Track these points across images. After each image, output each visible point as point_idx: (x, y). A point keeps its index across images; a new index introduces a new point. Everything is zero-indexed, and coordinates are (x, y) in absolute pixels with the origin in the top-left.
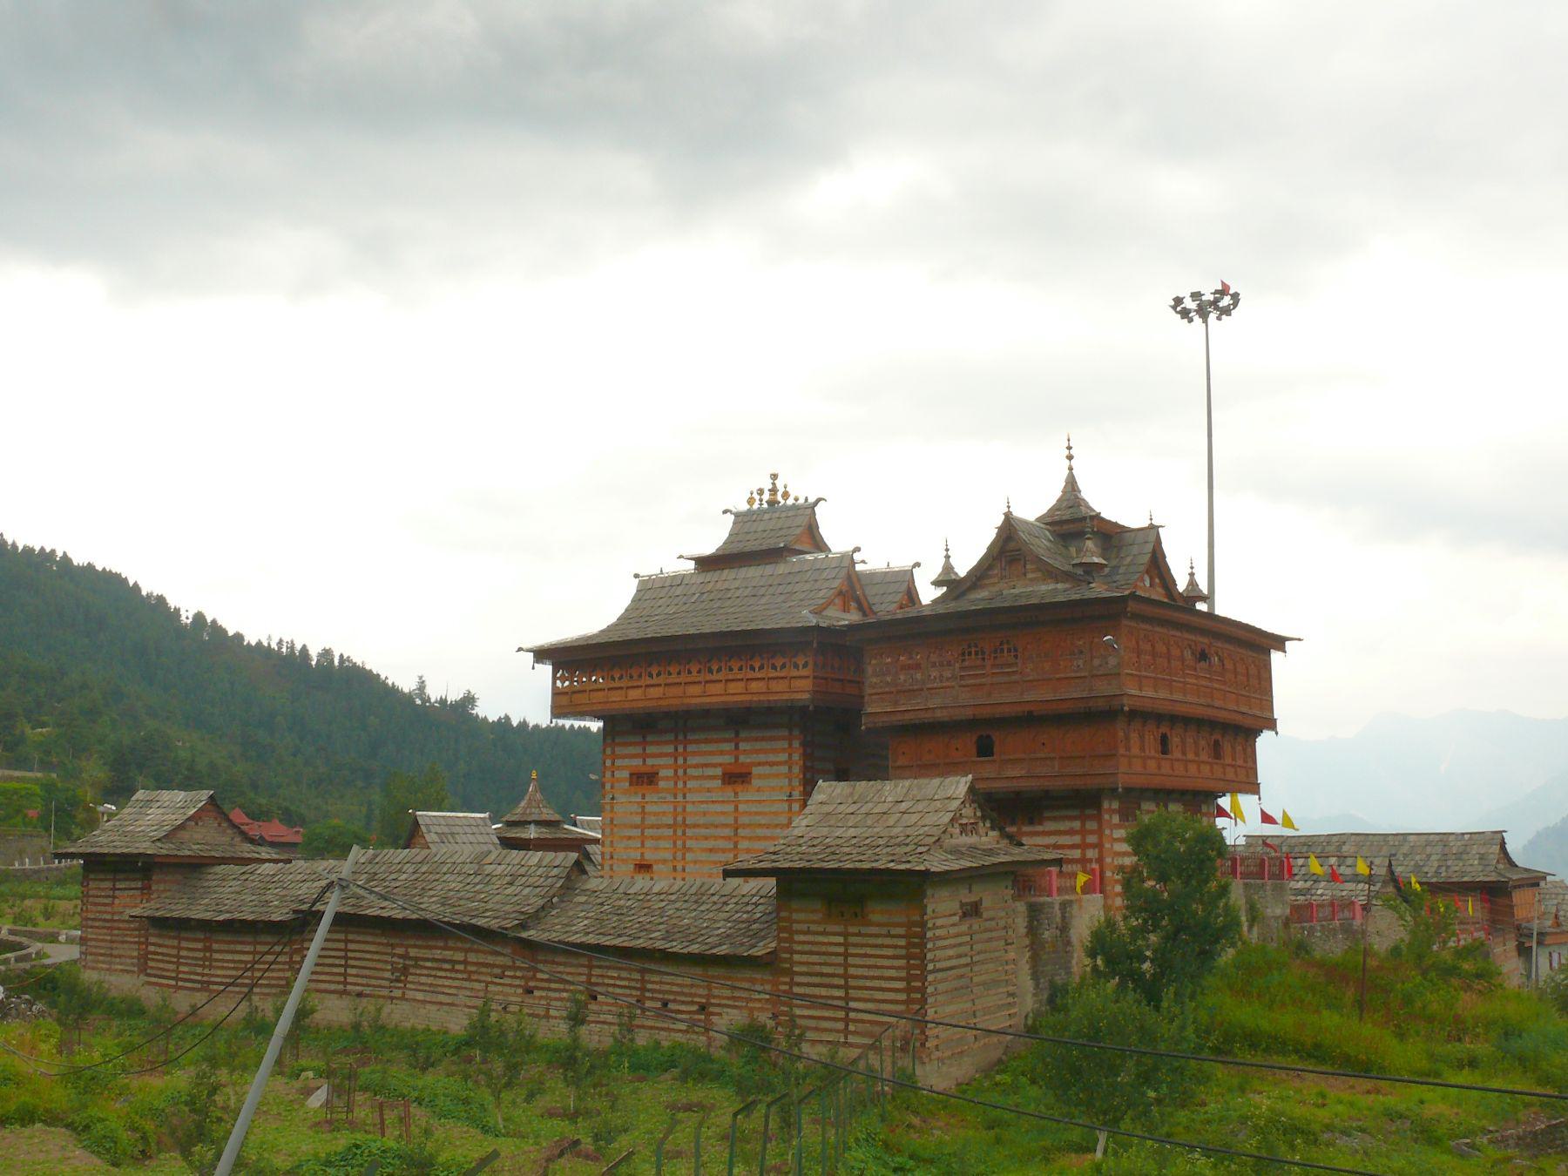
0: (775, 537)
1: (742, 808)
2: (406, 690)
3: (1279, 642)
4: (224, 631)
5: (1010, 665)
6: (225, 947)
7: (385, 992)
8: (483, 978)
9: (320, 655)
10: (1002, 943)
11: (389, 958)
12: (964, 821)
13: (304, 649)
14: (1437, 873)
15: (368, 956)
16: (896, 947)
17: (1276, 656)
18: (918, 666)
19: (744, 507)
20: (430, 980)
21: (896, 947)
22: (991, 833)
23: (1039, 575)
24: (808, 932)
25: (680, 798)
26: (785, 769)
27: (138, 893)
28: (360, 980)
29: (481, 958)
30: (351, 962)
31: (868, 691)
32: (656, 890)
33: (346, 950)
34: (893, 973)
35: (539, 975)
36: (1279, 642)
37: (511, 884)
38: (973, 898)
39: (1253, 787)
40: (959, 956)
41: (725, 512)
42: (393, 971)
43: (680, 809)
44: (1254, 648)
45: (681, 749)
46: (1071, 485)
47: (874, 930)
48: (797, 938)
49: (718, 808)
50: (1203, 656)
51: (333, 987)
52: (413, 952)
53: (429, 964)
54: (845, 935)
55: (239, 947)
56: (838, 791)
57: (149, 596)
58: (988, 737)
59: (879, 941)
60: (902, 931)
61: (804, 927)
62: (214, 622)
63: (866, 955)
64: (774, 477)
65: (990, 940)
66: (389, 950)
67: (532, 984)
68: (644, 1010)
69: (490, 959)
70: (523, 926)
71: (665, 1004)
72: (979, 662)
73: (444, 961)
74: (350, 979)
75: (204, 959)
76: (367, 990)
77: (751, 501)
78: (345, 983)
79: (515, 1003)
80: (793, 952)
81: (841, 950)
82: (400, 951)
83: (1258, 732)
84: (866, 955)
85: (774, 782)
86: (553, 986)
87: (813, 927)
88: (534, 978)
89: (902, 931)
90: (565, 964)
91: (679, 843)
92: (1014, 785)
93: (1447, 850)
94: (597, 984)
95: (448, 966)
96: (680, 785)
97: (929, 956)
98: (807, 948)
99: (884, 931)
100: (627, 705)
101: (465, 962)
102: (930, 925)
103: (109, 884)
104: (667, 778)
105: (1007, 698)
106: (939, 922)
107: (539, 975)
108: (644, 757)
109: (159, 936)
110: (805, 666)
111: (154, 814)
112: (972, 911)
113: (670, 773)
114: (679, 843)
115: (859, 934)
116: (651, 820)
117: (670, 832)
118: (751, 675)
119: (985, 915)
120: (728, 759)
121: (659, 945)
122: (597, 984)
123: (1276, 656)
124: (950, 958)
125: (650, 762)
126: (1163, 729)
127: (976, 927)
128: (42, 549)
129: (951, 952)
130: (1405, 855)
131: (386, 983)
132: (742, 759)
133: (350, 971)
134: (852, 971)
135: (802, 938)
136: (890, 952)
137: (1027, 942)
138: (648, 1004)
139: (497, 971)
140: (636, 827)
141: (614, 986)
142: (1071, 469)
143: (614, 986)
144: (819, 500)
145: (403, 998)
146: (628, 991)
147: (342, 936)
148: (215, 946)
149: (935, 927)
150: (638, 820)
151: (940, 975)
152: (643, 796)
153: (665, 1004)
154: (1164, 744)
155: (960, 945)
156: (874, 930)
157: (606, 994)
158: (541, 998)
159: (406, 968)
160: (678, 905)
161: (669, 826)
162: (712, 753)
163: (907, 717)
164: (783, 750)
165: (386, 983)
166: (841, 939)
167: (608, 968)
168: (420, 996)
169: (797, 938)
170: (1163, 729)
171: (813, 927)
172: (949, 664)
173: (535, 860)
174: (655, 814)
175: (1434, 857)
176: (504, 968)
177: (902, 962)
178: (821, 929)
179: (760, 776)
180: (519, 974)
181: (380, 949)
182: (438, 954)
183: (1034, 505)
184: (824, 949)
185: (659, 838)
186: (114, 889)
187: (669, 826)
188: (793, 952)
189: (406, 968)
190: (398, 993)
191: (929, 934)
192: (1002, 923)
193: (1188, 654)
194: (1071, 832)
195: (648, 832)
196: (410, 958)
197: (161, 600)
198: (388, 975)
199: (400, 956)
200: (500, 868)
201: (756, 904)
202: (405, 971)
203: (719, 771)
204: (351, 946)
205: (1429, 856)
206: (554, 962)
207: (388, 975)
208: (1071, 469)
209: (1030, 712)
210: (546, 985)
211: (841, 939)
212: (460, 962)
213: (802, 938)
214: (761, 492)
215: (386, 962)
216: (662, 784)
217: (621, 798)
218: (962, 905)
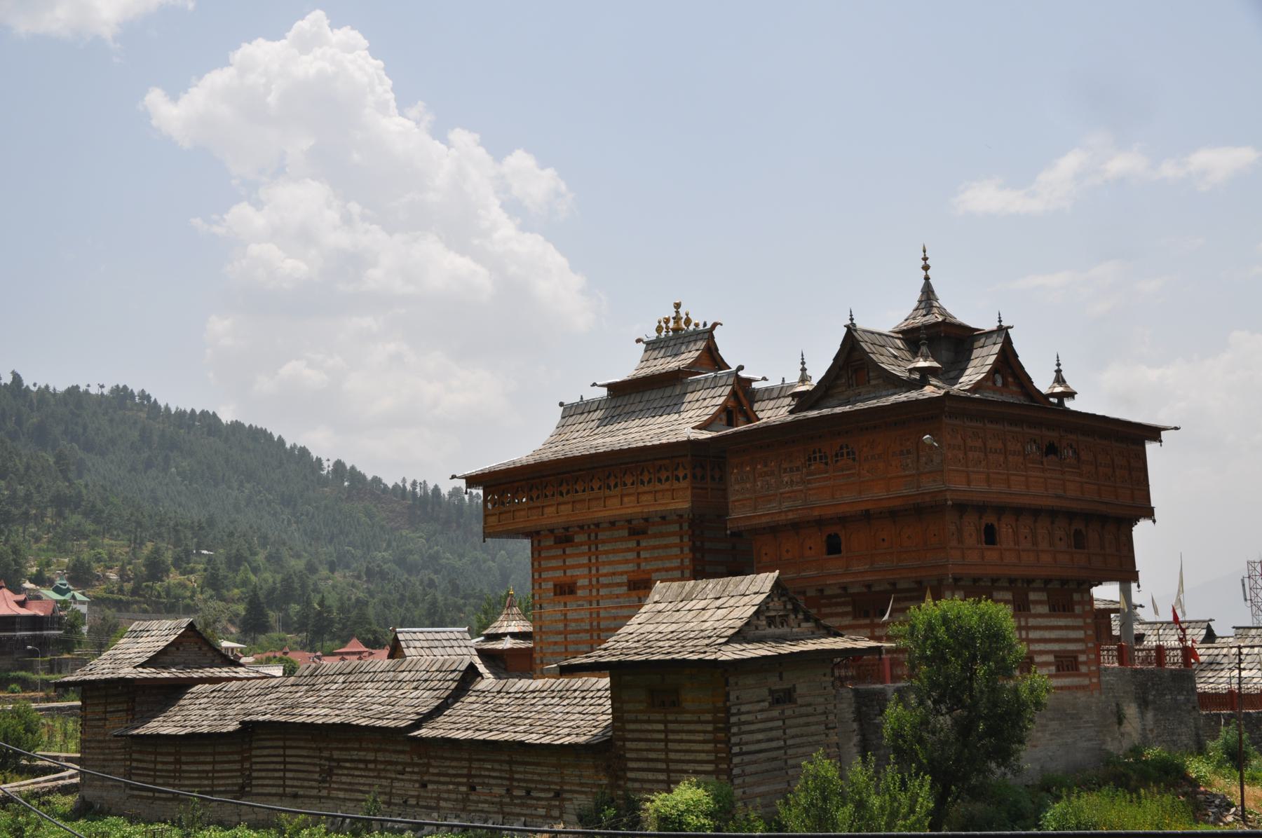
0: (686, 356)
3: (1154, 433)
4: (364, 477)
6: (190, 759)
7: (314, 792)
8: (389, 775)
9: (451, 495)
10: (823, 727)
11: (316, 761)
12: (772, 614)
15: (301, 760)
16: (705, 732)
17: (1151, 448)
19: (653, 335)
20: (348, 780)
21: (705, 732)
22: (804, 625)
23: (881, 381)
24: (636, 721)
25: (594, 605)
27: (123, 714)
28: (296, 783)
29: (388, 757)
30: (289, 766)
31: (732, 499)
32: (531, 688)
33: (285, 756)
34: (703, 756)
35: (432, 770)
36: (1154, 433)
37: (416, 688)
40: (771, 740)
41: (638, 341)
42: (320, 773)
43: (594, 615)
46: (928, 294)
47: (687, 717)
51: (274, 790)
52: (336, 754)
53: (348, 765)
55: (202, 758)
57: (294, 447)
58: (837, 535)
59: (692, 727)
60: (708, 717)
61: (632, 716)
62: (353, 468)
64: (677, 306)
65: (807, 725)
66: (317, 754)
67: (426, 778)
68: (513, 797)
69: (394, 758)
70: (417, 725)
71: (528, 793)
73: (360, 761)
74: (288, 782)
75: (174, 771)
76: (301, 792)
77: (659, 329)
78: (284, 786)
79: (412, 796)
80: (625, 740)
81: (662, 736)
82: (326, 754)
86: (442, 779)
87: (641, 717)
88: (427, 772)
89: (708, 717)
90: (452, 759)
94: (475, 776)
95: (362, 766)
96: (594, 592)
97: (734, 740)
98: (636, 735)
101: (375, 761)
102: (734, 710)
103: (100, 709)
104: (583, 587)
106: (744, 708)
107: (432, 770)
108: (565, 568)
109: (140, 752)
110: (685, 477)
112: (783, 698)
113: (586, 582)
115: (676, 722)
119: (799, 701)
122: (475, 776)
123: (1151, 448)
125: (569, 573)
126: (990, 519)
127: (788, 712)
128: (193, 411)
129: (760, 736)
131: (314, 784)
132: (643, 565)
133: (289, 775)
134: (672, 756)
135: (632, 726)
136: (701, 737)
138: (516, 793)
139: (400, 768)
140: (560, 633)
141: (490, 777)
142: (927, 278)
143: (490, 777)
144: (715, 325)
145: (328, 798)
146: (499, 782)
147: (281, 743)
148: (184, 759)
149: (739, 713)
150: (561, 626)
151: (747, 758)
152: (565, 605)
153: (528, 793)
154: (990, 536)
155: (771, 729)
156: (687, 717)
157: (483, 784)
158: (433, 791)
159: (331, 769)
160: (545, 701)
161: (586, 631)
162: (619, 562)
163: (764, 520)
165: (314, 784)
166: (661, 727)
167: (484, 760)
168: (341, 795)
171: (641, 717)
174: (576, 620)
176: (405, 764)
177: (710, 747)
178: (645, 718)
180: (416, 770)
181: (311, 753)
182: (355, 755)
183: (888, 313)
186: (106, 712)
187: (586, 631)
188: (625, 740)
189: (331, 769)
190: (324, 793)
191: (733, 719)
192: (820, 709)
195: (571, 637)
196: (334, 760)
197: (304, 452)
198: (316, 776)
199: (326, 759)
202: (330, 772)
203: (624, 579)
204: (289, 752)
206: (443, 758)
207: (316, 776)
208: (927, 278)
210: (436, 779)
211: (661, 727)
212: (371, 762)
213: (632, 726)
214: (667, 321)
215: (314, 765)
216: (580, 593)
218: (771, 692)
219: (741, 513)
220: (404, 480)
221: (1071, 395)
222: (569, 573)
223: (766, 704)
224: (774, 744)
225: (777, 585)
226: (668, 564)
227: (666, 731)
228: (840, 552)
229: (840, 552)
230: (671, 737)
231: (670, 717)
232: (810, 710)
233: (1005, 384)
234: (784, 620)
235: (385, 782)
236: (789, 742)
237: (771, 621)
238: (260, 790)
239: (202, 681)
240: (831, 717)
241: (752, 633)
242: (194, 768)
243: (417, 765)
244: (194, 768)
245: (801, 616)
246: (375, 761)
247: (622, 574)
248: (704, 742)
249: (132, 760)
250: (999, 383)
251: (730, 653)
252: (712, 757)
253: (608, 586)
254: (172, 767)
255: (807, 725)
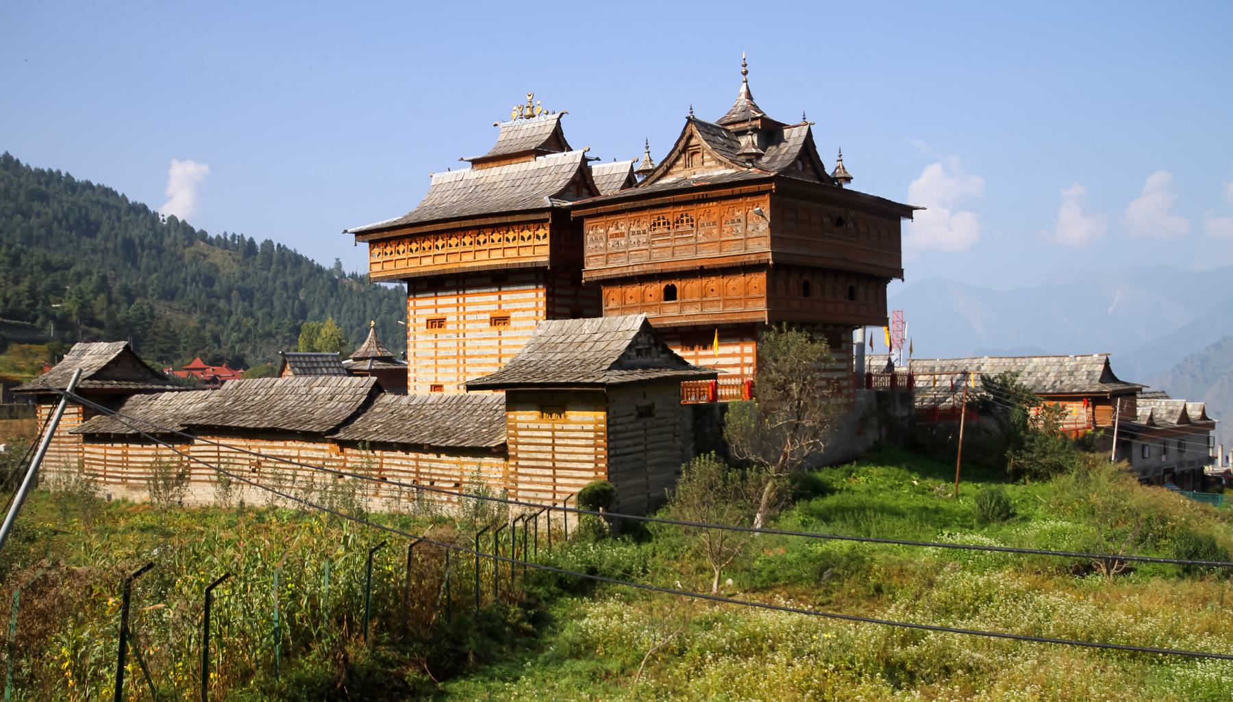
1: (503, 342)
2: (327, 268)
3: (907, 211)
4: (192, 230)
5: (688, 232)
9: (262, 245)
13: (251, 240)
14: (1053, 387)
16: (587, 439)
17: (905, 223)
18: (622, 235)
21: (587, 439)
24: (528, 429)
26: (533, 313)
36: (907, 211)
38: (647, 402)
39: (882, 321)
40: (636, 445)
44: (891, 215)
45: (461, 300)
48: (521, 433)
49: (488, 343)
50: (840, 222)
52: (263, 451)
54: (553, 431)
56: (553, 327)
60: (591, 427)
61: (525, 426)
63: (567, 445)
65: (661, 433)
71: (432, 483)
72: (666, 230)
80: (517, 444)
81: (550, 441)
83: (888, 280)
84: (567, 445)
85: (525, 323)
91: (461, 369)
92: (691, 321)
93: (1062, 369)
96: (461, 327)
99: (579, 427)
100: (422, 270)
104: (452, 323)
105: (685, 257)
110: (545, 236)
111: (87, 360)
113: (455, 318)
114: (461, 369)
115: (562, 430)
116: (442, 353)
117: (455, 361)
118: (507, 245)
119: (657, 415)
120: (494, 307)
121: (427, 441)
123: (905, 223)
124: (628, 446)
125: (440, 310)
128: (50, 170)
129: (629, 442)
130: (1029, 373)
132: (504, 307)
136: (583, 442)
137: (692, 435)
154: (852, 295)
159: (259, 463)
161: (454, 357)
162: (483, 304)
163: (614, 272)
164: (532, 300)
166: (549, 434)
169: (521, 433)
170: (806, 277)
171: (532, 426)
172: (644, 232)
173: (347, 383)
174: (445, 349)
175: (1052, 374)
177: (591, 450)
178: (536, 426)
179: (516, 319)
184: (538, 441)
185: (446, 366)
187: (454, 357)
188: (517, 444)
189: (259, 463)
193: (826, 220)
194: (733, 355)
200: (324, 389)
201: (497, 411)
203: (488, 316)
205: (1047, 374)
209: (702, 267)
211: (549, 434)
216: (449, 327)
217: (420, 338)
219: (594, 265)
220: (225, 234)
221: (848, 179)
222: (440, 310)
223: (633, 418)
224: (638, 448)
225: (127, 348)
226: (524, 306)
227: (553, 438)
228: (675, 298)
229: (675, 298)
230: (557, 441)
231: (558, 427)
232: (664, 422)
233: (804, 169)
234: (648, 351)
235: (306, 473)
236: (649, 447)
237: (639, 352)
238: (197, 477)
239: (139, 391)
240: (678, 428)
241: (626, 361)
242: (139, 459)
243: (335, 460)
244: (139, 459)
245: (660, 349)
246: (298, 457)
247: (485, 312)
248: (587, 446)
249: (83, 452)
250: (800, 168)
251: (615, 377)
252: (592, 458)
253: (472, 322)
254: (120, 459)
255: (661, 433)
